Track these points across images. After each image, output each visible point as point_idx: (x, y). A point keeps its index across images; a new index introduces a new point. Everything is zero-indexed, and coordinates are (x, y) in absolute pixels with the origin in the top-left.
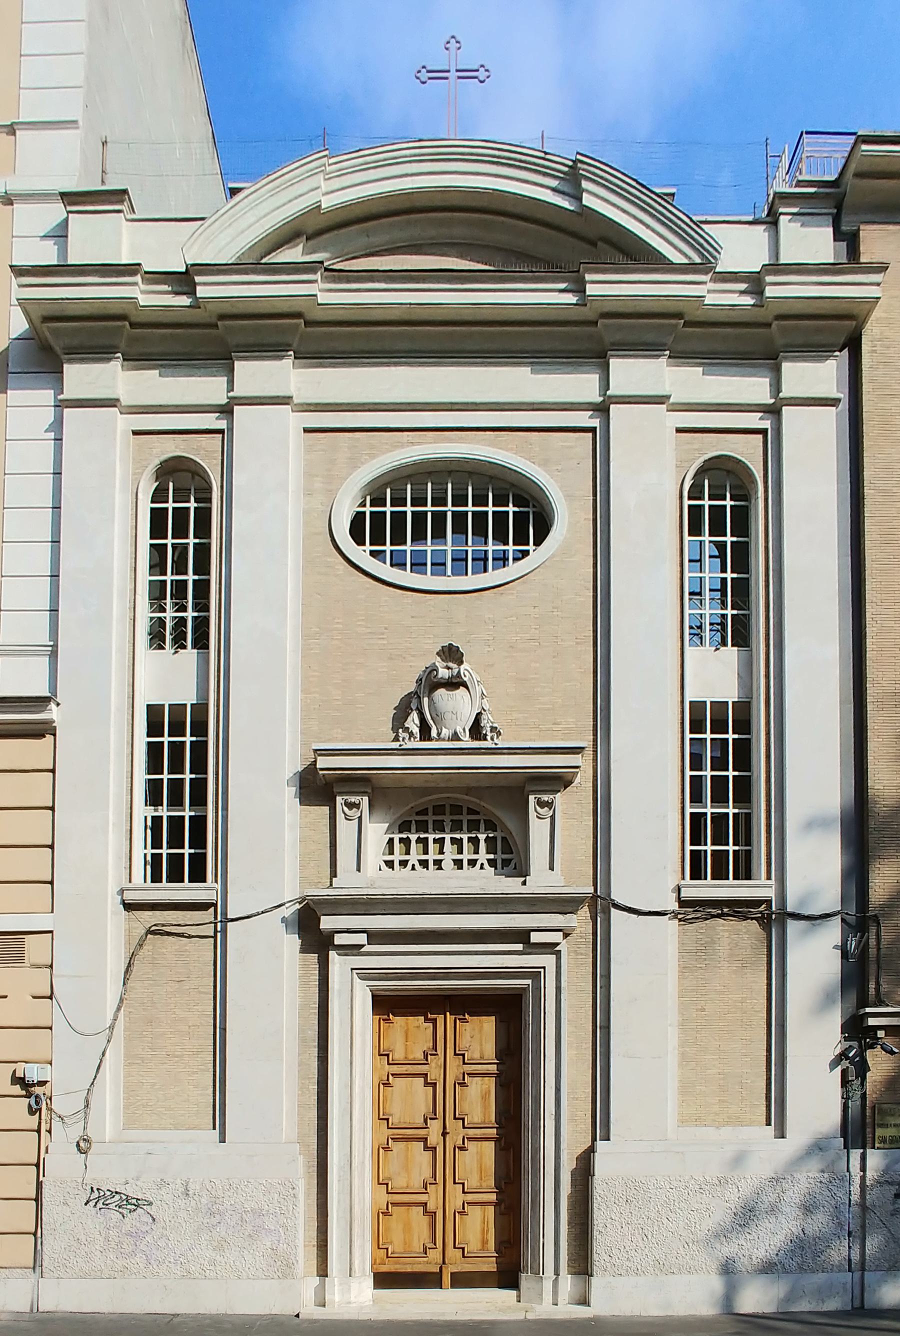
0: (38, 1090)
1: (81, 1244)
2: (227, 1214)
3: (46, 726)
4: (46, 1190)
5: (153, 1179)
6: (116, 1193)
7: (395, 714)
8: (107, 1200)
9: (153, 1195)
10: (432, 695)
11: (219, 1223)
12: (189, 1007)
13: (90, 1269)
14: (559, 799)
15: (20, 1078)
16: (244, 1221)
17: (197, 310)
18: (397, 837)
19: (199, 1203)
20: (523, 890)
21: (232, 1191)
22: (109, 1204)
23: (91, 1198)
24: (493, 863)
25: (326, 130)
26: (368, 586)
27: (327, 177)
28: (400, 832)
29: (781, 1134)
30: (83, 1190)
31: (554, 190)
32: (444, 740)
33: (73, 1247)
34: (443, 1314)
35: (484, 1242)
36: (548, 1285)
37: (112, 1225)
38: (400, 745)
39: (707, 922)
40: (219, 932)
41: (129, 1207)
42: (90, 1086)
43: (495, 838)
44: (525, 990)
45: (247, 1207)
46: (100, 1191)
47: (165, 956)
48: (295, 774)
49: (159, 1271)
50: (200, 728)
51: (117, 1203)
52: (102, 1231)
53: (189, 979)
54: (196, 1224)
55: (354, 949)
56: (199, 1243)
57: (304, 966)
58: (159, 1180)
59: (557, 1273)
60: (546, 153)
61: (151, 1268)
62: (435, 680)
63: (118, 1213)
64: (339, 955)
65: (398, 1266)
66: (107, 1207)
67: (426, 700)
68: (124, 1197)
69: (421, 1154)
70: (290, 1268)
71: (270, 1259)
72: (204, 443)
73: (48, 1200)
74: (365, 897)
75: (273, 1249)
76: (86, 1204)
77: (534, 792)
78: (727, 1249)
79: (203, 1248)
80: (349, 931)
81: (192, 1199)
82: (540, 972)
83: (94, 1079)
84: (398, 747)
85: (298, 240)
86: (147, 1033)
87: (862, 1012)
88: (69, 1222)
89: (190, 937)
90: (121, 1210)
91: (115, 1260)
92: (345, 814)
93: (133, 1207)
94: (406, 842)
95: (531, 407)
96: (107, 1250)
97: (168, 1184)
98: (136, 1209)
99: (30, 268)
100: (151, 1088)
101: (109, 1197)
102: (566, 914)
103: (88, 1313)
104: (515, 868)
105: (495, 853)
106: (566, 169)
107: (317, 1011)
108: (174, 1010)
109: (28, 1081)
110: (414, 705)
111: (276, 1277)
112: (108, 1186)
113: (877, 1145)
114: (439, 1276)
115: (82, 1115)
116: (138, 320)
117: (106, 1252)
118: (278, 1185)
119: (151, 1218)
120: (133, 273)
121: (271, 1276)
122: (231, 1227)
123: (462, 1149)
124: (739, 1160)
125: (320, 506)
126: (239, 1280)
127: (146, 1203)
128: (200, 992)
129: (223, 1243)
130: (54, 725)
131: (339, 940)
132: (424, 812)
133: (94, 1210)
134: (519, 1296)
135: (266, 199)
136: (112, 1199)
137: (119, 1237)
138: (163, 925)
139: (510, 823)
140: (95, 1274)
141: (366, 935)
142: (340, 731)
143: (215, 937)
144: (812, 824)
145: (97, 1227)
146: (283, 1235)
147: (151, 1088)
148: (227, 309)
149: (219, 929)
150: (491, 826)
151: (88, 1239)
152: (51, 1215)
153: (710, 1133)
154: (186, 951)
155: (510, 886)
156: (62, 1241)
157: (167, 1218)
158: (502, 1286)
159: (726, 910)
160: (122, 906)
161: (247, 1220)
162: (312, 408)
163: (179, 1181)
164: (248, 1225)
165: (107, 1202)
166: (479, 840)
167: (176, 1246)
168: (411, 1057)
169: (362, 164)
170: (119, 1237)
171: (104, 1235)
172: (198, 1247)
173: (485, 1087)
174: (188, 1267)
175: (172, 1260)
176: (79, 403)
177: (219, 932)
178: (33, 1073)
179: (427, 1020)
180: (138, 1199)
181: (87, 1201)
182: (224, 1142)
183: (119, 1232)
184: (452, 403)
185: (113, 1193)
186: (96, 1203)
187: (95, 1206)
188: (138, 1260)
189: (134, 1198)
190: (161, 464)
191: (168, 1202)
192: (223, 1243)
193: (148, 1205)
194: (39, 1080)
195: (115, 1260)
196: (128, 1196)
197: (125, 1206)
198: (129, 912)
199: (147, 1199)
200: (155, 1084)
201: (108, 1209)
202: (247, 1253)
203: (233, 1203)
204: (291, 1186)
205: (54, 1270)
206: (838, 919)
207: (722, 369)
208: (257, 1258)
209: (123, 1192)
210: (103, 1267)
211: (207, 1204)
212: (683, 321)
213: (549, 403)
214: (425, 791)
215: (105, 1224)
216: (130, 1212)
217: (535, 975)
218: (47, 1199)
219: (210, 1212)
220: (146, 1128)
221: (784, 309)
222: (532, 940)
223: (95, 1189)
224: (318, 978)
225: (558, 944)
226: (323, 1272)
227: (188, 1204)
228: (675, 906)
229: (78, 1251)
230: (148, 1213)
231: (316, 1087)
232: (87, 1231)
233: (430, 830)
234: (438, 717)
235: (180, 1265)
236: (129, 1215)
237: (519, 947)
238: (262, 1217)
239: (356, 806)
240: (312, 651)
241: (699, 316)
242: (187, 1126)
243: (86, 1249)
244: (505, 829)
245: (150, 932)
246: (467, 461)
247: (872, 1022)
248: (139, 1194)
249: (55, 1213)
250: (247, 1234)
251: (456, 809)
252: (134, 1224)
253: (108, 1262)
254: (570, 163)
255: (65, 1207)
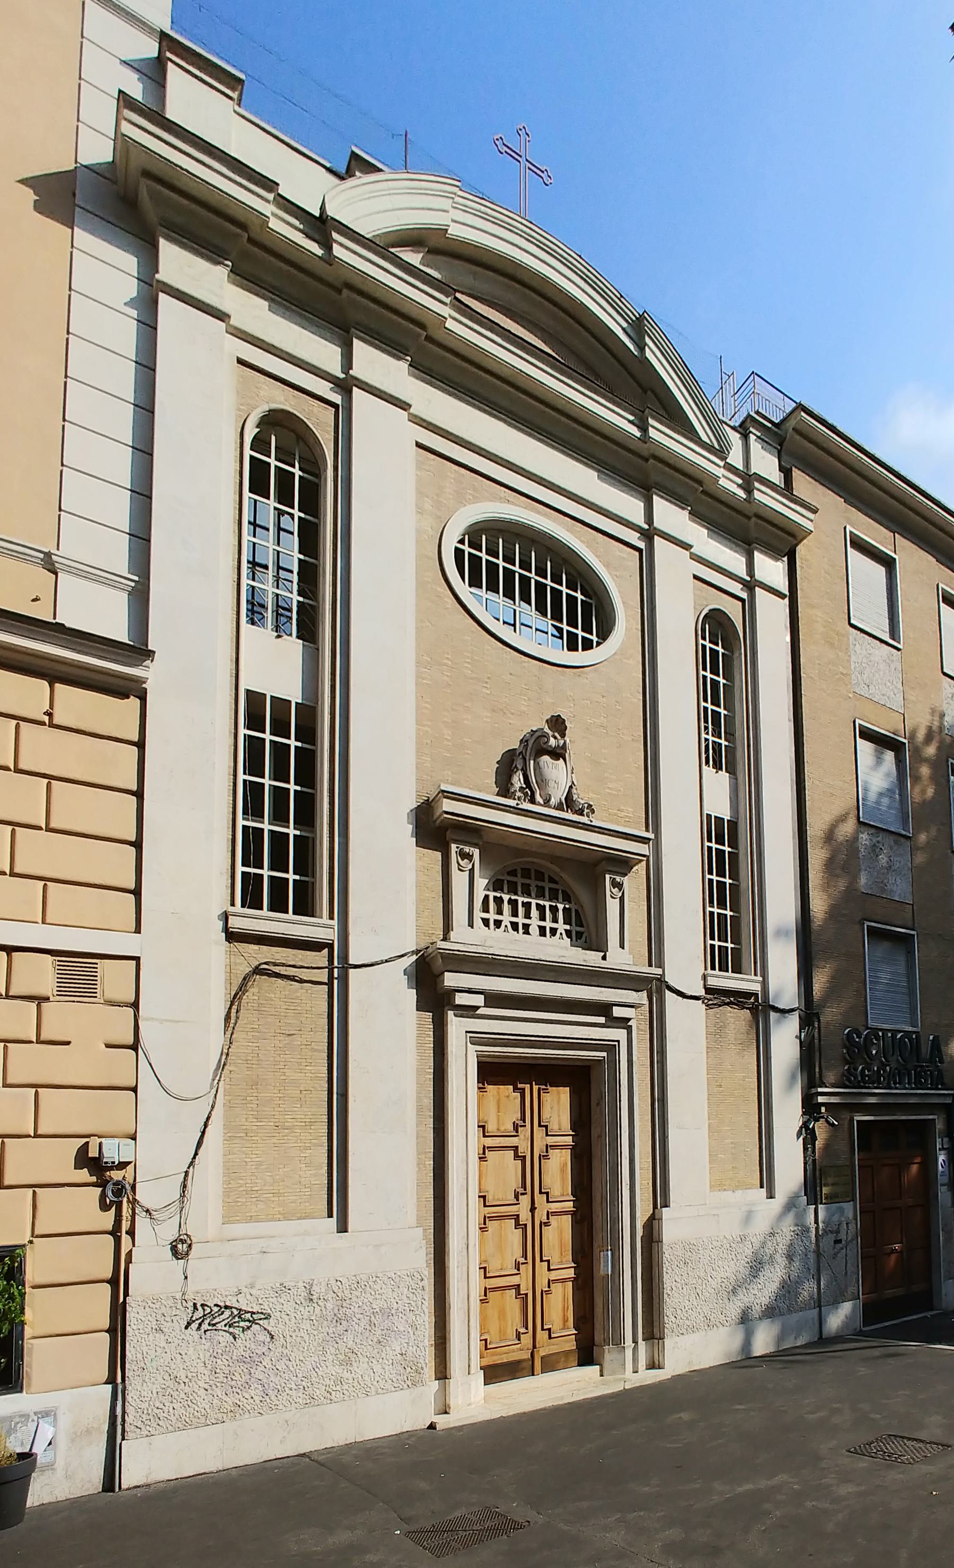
0: (116, 1175)
1: (179, 1383)
2: (354, 1319)
3: (132, 685)
4: (133, 1314)
5: (271, 1285)
6: (226, 1307)
7: (497, 768)
8: (214, 1318)
9: (271, 1304)
10: (538, 760)
11: (346, 1331)
12: (301, 1067)
13: (191, 1416)
14: (626, 881)
15: (94, 1159)
16: (372, 1325)
17: (328, 266)
18: (492, 894)
19: (323, 1309)
20: (604, 964)
21: (360, 1290)
22: (217, 1323)
23: (194, 1319)
24: (568, 933)
25: (409, 136)
26: (474, 630)
27: (454, 205)
28: (495, 890)
29: (771, 1196)
30: (183, 1309)
31: (623, 329)
32: (550, 807)
33: (169, 1390)
34: (562, 1398)
35: (565, 1321)
36: (629, 1353)
37: (220, 1351)
38: (517, 804)
39: (721, 1008)
40: (336, 978)
41: (242, 1324)
42: (189, 1168)
43: (569, 909)
44: (600, 1062)
45: (376, 1307)
46: (206, 1308)
47: (273, 1003)
48: (412, 811)
49: (278, 1403)
50: (308, 732)
51: (226, 1322)
52: (207, 1362)
53: (301, 1033)
54: (321, 1336)
55: (469, 1011)
56: (324, 1359)
57: (420, 1026)
58: (278, 1285)
59: (635, 1341)
60: (622, 296)
61: (268, 1401)
62: (545, 747)
63: (228, 1334)
64: (456, 1015)
65: (495, 1358)
66: (214, 1328)
67: (532, 762)
68: (236, 1312)
69: (513, 1233)
70: (420, 1373)
71: (399, 1365)
72: (315, 410)
73: (135, 1327)
74: (490, 956)
75: (402, 1355)
76: (186, 1328)
77: (610, 872)
78: (744, 1299)
79: (328, 1365)
80: (470, 991)
81: (315, 1305)
82: (615, 1045)
83: (194, 1158)
84: (515, 805)
85: (421, 249)
86: (252, 1098)
87: (813, 1091)
88: (164, 1355)
89: (302, 981)
90: (231, 1330)
91: (224, 1397)
92: (459, 864)
93: (247, 1324)
94: (499, 901)
95: (599, 510)
96: (214, 1387)
97: (289, 1289)
98: (251, 1326)
99: (148, 110)
100: (256, 1168)
101: (217, 1315)
102: (638, 991)
103: (190, 1477)
104: (586, 942)
105: (570, 925)
106: (634, 319)
107: (432, 1077)
108: (284, 1070)
109: (106, 1163)
110: (520, 764)
111: (406, 1386)
112: (216, 1298)
113: (824, 1201)
114: (531, 1363)
115: (175, 1208)
116: (258, 238)
117: (213, 1390)
118: (406, 1277)
119: (268, 1336)
120: (270, 190)
121: (401, 1387)
122: (359, 1335)
123: (547, 1224)
124: (748, 1217)
125: (430, 529)
126: (369, 1398)
127: (263, 1316)
128: (313, 1050)
129: (350, 1355)
130: (144, 686)
131: (461, 999)
132: (513, 873)
133: (196, 1335)
134: (601, 1371)
135: (402, 194)
136: (221, 1317)
137: (229, 1366)
138: (275, 964)
139: (583, 895)
140: (198, 1421)
141: (483, 996)
142: (450, 773)
143: (330, 984)
144: (779, 933)
145: (201, 1357)
146: (412, 1335)
147: (256, 1168)
148: (357, 281)
149: (336, 975)
150: (567, 898)
151: (190, 1375)
152: (138, 1349)
153: (728, 1196)
154: (297, 998)
155: (591, 959)
156: (153, 1383)
157: (287, 1332)
158: (581, 1363)
159: (732, 999)
160: (224, 934)
161: (376, 1322)
162: (424, 424)
163: (301, 1284)
164: (376, 1329)
165: (214, 1322)
166: (503, 901)
167: (299, 1366)
168: (502, 1129)
169: (476, 210)
170: (229, 1366)
171: (210, 1367)
172: (322, 1364)
173: (563, 1159)
174: (312, 1392)
175: (294, 1387)
176: (177, 294)
177: (336, 978)
178: (112, 1151)
179: (516, 1089)
180: (253, 1313)
181: (188, 1323)
182: (346, 1231)
183: (229, 1359)
184: (541, 478)
185: (221, 1308)
186: (200, 1325)
187: (199, 1328)
188: (252, 1393)
189: (249, 1312)
190: (269, 411)
191: (288, 1312)
192: (350, 1355)
193: (265, 1319)
194: (121, 1160)
195: (224, 1397)
196: (240, 1310)
197: (237, 1324)
198: (230, 943)
199: (264, 1312)
200: (261, 1163)
201: (216, 1330)
202: (376, 1363)
203: (361, 1303)
204: (420, 1278)
205: (142, 1426)
206: (797, 1013)
207: (720, 539)
208: (387, 1368)
209: (234, 1306)
210: (209, 1411)
211: (333, 1309)
212: (701, 489)
213: (611, 513)
214: (518, 852)
215: (211, 1351)
216: (243, 1331)
217: (611, 1048)
218: (133, 1326)
219: (336, 1318)
220: (251, 1219)
221: (762, 512)
222: (615, 1015)
223: (199, 1306)
224: (432, 1039)
225: (629, 1019)
226: (442, 1373)
227: (312, 1312)
228: (702, 992)
229: (175, 1394)
230: (265, 1329)
231: (432, 1163)
232: (188, 1364)
233: (506, 890)
234: (543, 782)
235: (302, 1391)
236: (242, 1335)
237: (602, 1020)
238: (391, 1317)
239: (469, 857)
240: (424, 681)
241: (711, 489)
242: (299, 1215)
243: (187, 1389)
244: (578, 902)
245: (258, 971)
246: (551, 538)
247: (821, 1099)
248: (254, 1305)
249: (144, 1345)
250: (375, 1340)
251: (540, 876)
252: (248, 1346)
253: (215, 1401)
254: (638, 316)
255: (157, 1335)
